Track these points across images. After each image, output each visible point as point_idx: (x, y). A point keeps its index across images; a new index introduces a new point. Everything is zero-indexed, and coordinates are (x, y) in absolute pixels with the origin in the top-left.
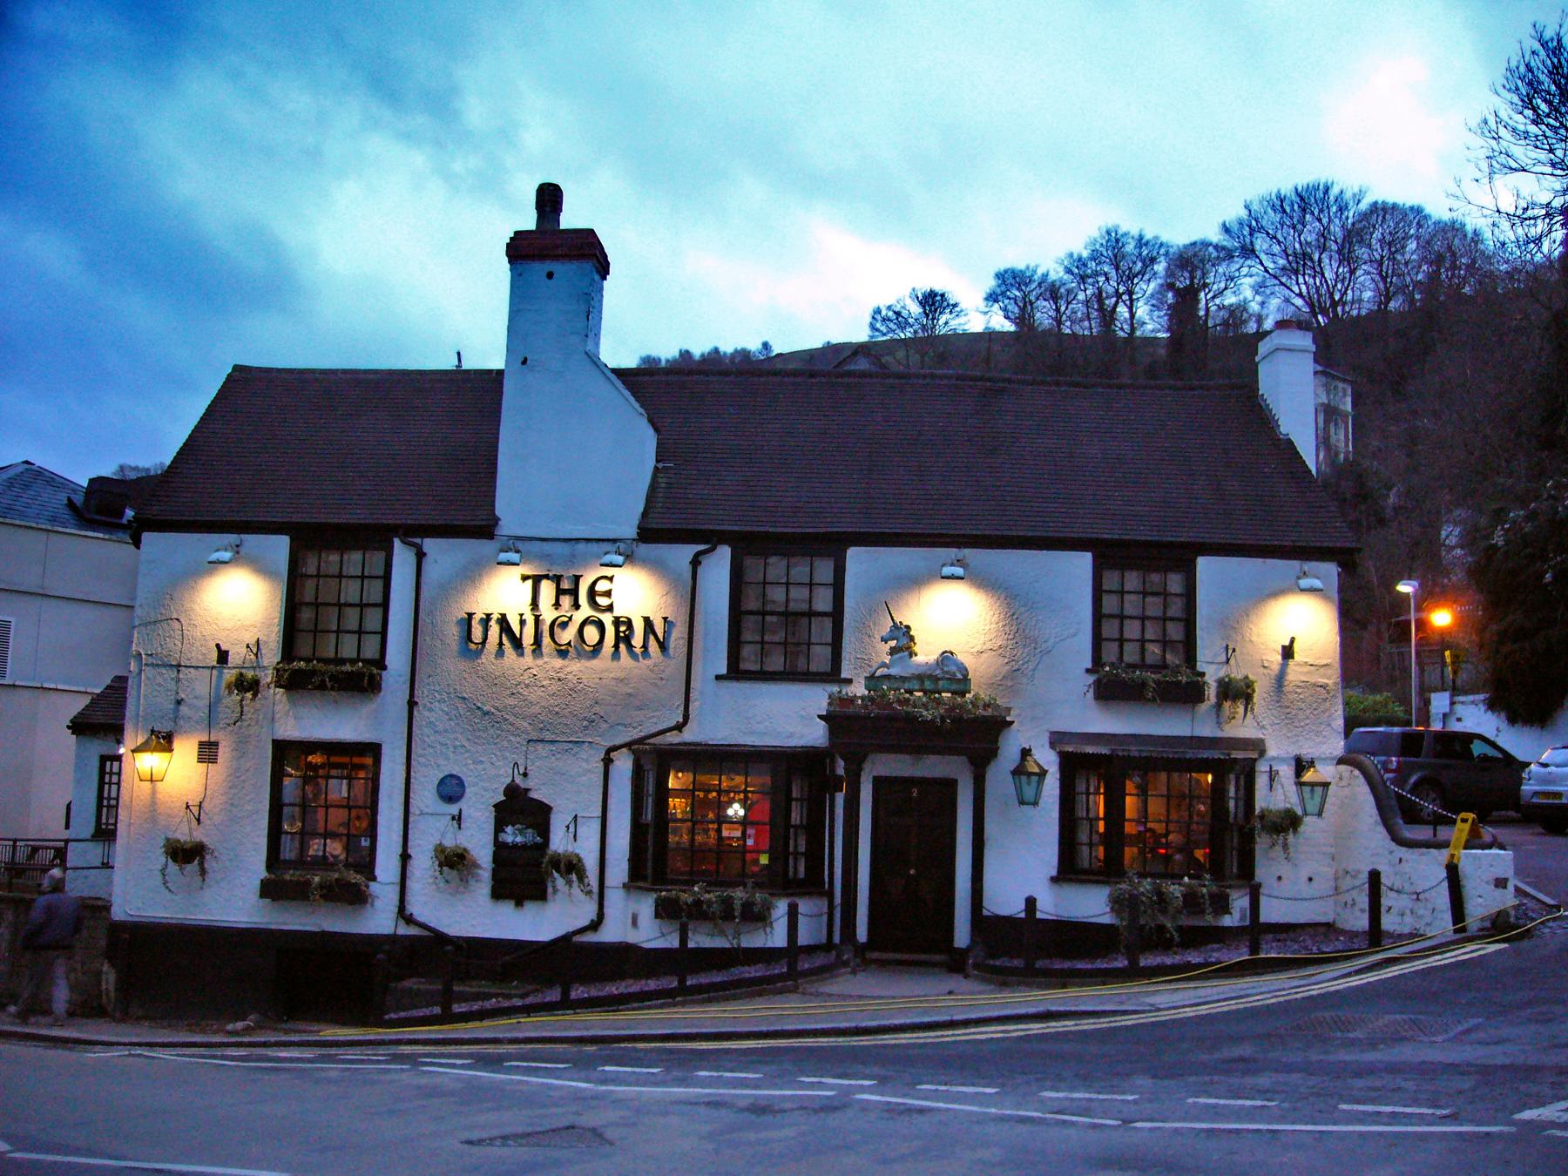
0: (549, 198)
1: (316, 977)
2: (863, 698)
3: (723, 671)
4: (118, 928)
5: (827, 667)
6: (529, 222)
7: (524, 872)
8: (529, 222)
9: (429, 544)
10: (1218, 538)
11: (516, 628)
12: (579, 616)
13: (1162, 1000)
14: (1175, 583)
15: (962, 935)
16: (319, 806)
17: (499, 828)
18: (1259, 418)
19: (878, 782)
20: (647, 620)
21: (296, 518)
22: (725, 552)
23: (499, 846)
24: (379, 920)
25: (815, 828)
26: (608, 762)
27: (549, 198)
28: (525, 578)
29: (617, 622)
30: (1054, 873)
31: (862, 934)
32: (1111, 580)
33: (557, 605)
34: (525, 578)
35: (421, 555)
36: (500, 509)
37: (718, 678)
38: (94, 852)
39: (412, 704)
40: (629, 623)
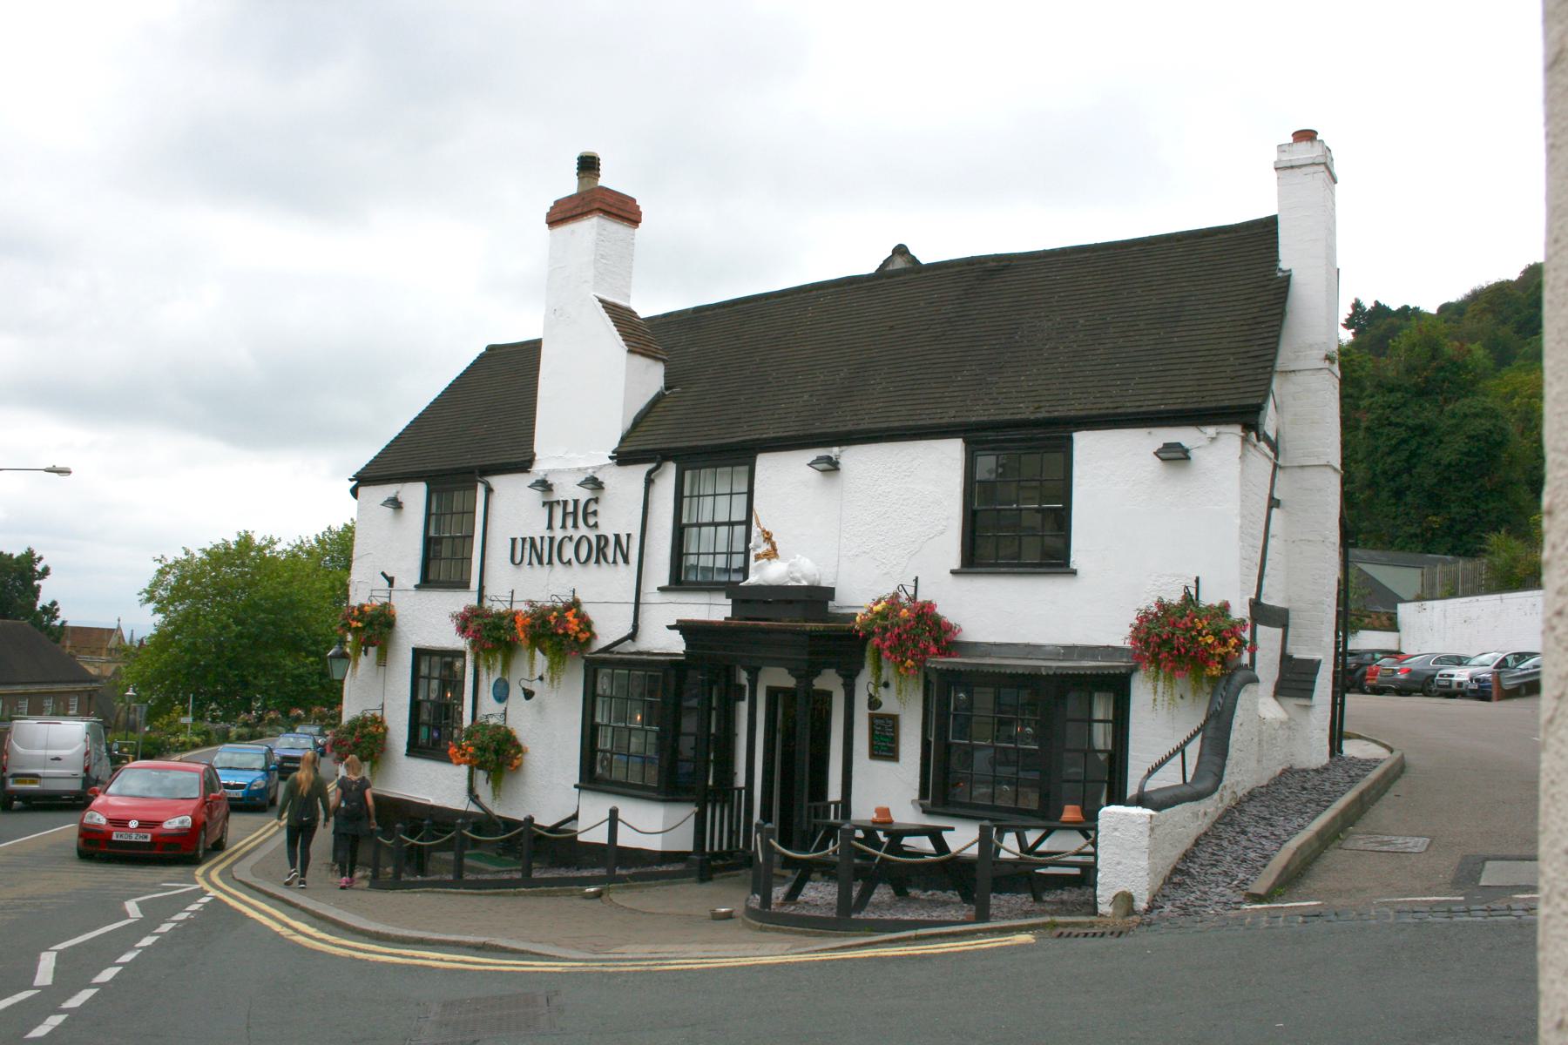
0: (588, 165)
3: (666, 583)
6: (569, 184)
10: (1106, 406)
13: (632, 950)
19: (773, 693)
20: (617, 537)
21: (430, 467)
22: (671, 470)
27: (588, 165)
29: (599, 537)
33: (564, 526)
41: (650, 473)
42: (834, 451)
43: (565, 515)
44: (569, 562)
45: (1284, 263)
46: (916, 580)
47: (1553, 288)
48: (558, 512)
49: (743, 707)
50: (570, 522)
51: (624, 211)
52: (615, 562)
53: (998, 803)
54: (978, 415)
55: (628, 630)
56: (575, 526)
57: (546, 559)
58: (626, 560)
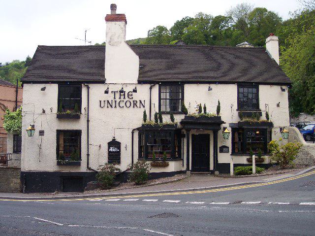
0: (113, 7)
1: (70, 176)
2: (64, 136)
4: (23, 173)
6: (109, 12)
7: (114, 157)
8: (109, 12)
9: (90, 86)
11: (111, 103)
12: (125, 101)
14: (254, 90)
15: (212, 167)
16: (69, 144)
17: (109, 148)
18: (267, 55)
19: (193, 135)
23: (109, 152)
24: (83, 169)
26: (133, 133)
27: (113, 7)
31: (190, 169)
33: (120, 98)
35: (88, 88)
36: (106, 77)
38: (14, 156)
39: (88, 121)
46: (219, 102)
50: (122, 97)
51: (121, 18)
52: (140, 107)
53: (162, 44)
54: (241, 80)
55: (153, 90)
57: (114, 106)
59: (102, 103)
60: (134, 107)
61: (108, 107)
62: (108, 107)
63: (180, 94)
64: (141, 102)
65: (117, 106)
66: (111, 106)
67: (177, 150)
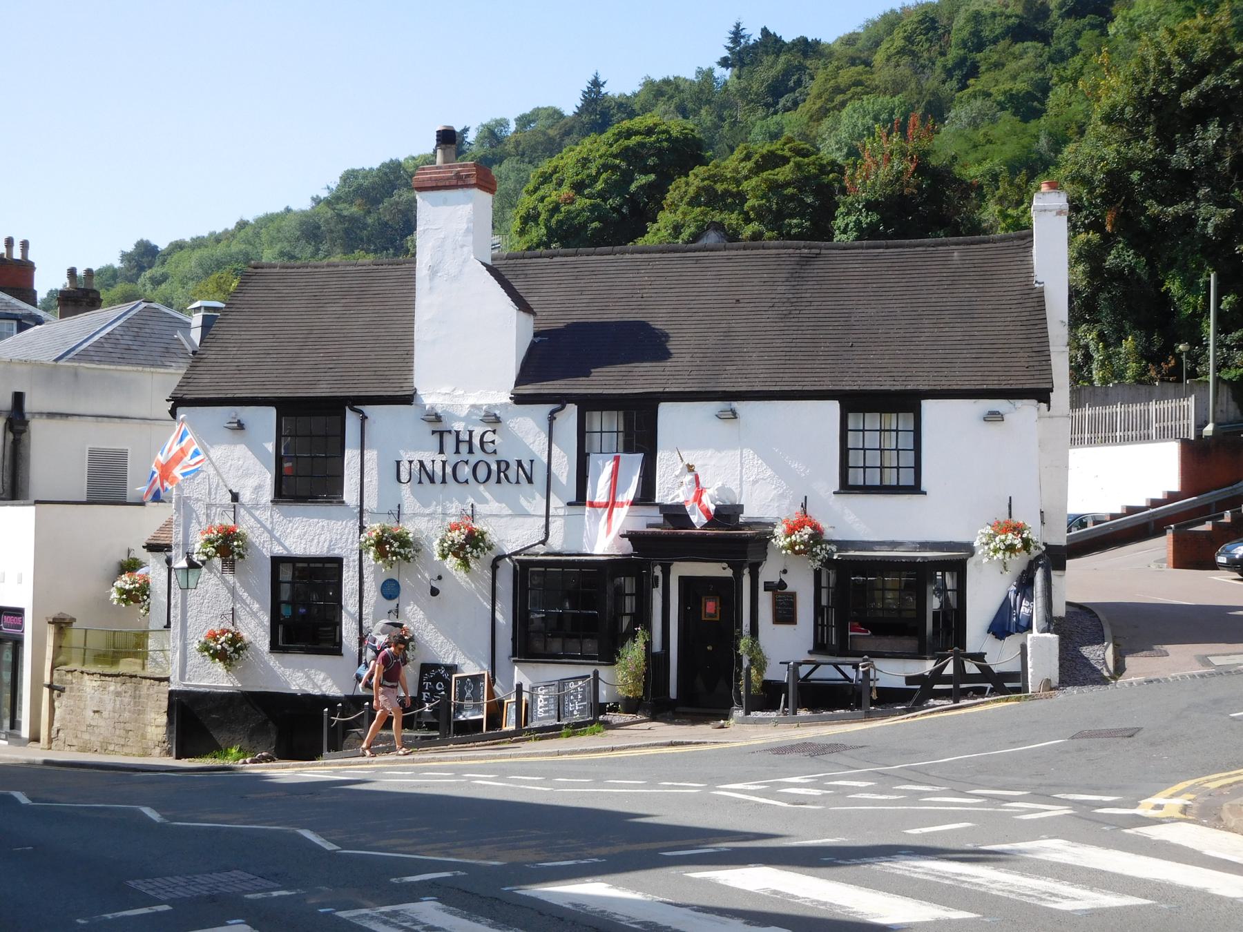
5: (851, 482)
9: (367, 409)
12: (473, 460)
14: (906, 421)
19: (683, 580)
25: (586, 775)
28: (434, 432)
30: (811, 648)
32: (854, 421)
33: (457, 452)
34: (434, 432)
35: (364, 418)
37: (569, 504)
40: (508, 465)
41: (552, 413)
42: (736, 405)
43: (458, 441)
44: (467, 482)
45: (206, 234)
47: (433, 271)
48: (450, 441)
49: (657, 595)
50: (464, 448)
52: (518, 482)
56: (471, 451)
58: (530, 480)
59: (404, 468)
60: (499, 481)
61: (420, 482)
62: (420, 482)
63: (312, 565)
64: (519, 463)
65: (494, 467)
66: (432, 481)
67: (1207, 526)
